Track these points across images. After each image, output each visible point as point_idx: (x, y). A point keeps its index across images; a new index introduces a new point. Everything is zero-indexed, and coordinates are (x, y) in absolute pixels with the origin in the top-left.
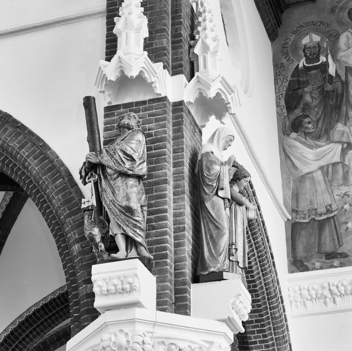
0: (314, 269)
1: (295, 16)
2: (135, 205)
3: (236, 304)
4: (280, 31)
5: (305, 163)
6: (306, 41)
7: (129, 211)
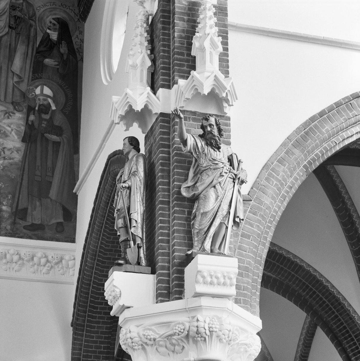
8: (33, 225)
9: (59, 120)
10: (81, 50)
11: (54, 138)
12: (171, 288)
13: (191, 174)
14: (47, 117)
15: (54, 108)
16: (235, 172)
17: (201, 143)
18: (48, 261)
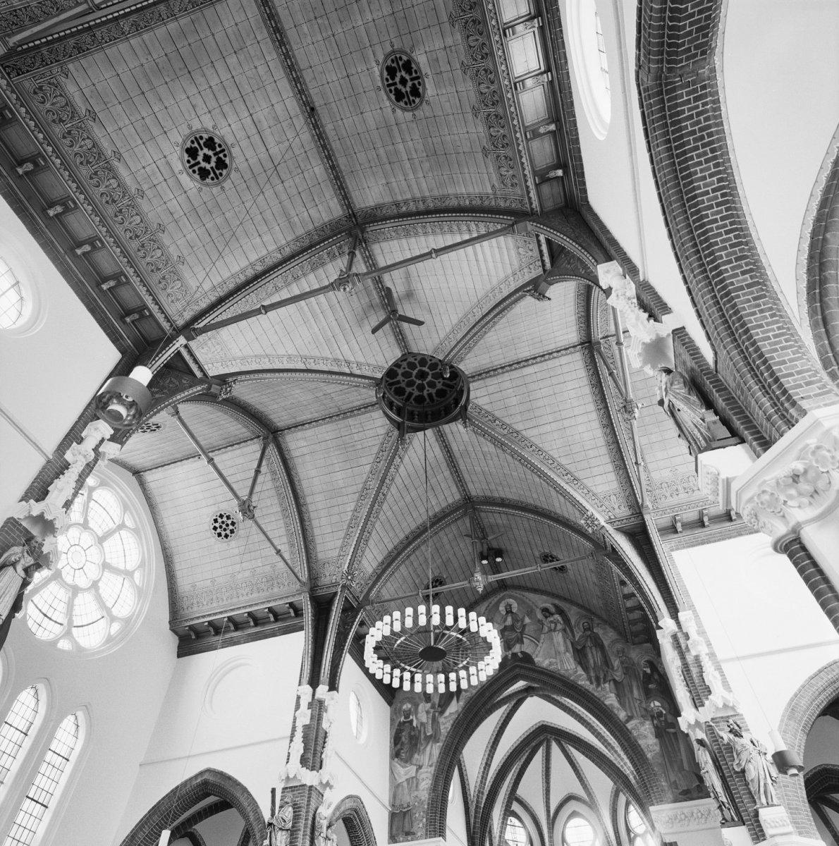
0: (400, 842)
4: (394, 701)
5: (400, 777)
6: (404, 707)
8: (684, 791)
10: (665, 674)
13: (735, 756)
14: (663, 719)
15: (664, 712)
16: (758, 748)
17: (732, 736)
18: (702, 814)
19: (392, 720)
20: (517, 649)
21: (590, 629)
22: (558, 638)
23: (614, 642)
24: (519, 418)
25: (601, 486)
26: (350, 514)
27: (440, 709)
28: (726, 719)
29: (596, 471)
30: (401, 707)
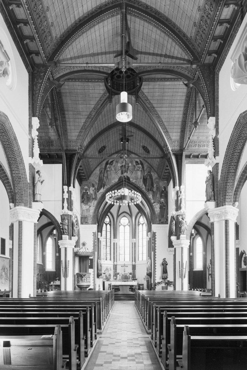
1: (84, 183)
2: (66, 228)
3: (31, 49)
6: (85, 187)
7: (66, 229)
9: (165, 204)
11: (164, 207)
12: (178, 238)
17: (182, 219)
19: (81, 191)
20: (125, 174)
21: (150, 172)
22: (139, 173)
23: (156, 178)
24: (156, 102)
25: (174, 137)
26: (83, 123)
27: (97, 190)
28: (182, 215)
29: (175, 130)
30: (84, 187)
